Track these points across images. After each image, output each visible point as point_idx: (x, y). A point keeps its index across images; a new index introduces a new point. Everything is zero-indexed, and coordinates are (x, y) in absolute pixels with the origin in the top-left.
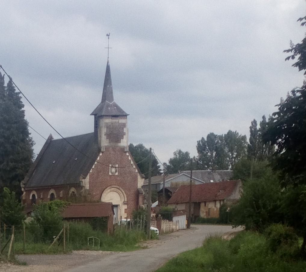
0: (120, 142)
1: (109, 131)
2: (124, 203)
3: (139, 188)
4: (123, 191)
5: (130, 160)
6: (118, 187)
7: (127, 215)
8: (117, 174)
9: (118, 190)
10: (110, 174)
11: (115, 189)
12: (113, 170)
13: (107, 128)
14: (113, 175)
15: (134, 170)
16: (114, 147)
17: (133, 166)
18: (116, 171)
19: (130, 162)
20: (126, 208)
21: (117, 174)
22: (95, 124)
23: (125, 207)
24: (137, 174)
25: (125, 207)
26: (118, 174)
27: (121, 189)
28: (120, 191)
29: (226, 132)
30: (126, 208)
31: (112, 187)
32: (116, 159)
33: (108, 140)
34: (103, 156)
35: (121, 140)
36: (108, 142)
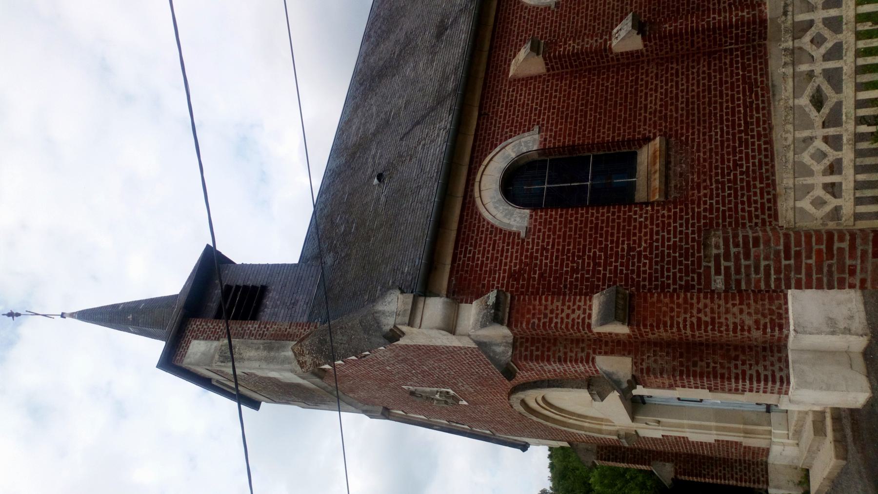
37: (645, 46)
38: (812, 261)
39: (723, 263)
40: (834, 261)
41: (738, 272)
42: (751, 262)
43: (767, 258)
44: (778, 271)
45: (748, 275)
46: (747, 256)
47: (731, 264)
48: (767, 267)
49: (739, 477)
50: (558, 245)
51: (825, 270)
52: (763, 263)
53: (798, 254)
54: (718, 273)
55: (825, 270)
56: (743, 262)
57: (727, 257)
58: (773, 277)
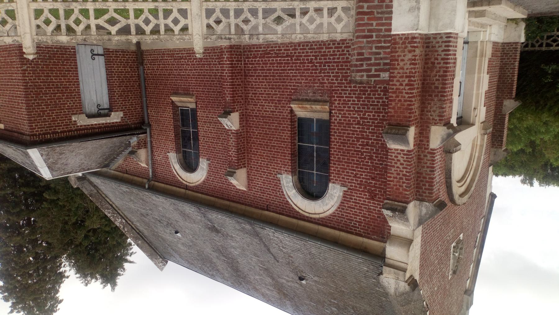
37: (237, 111)
38: (374, 23)
39: (373, 72)
40: (375, 11)
41: (379, 64)
42: (373, 57)
43: (371, 48)
44: (380, 42)
45: (381, 59)
46: (370, 59)
47: (373, 68)
48: (377, 48)
49: (513, 60)
51: (380, 16)
52: (374, 50)
53: (369, 31)
54: (378, 76)
55: (380, 16)
56: (373, 61)
57: (370, 70)
58: (383, 44)
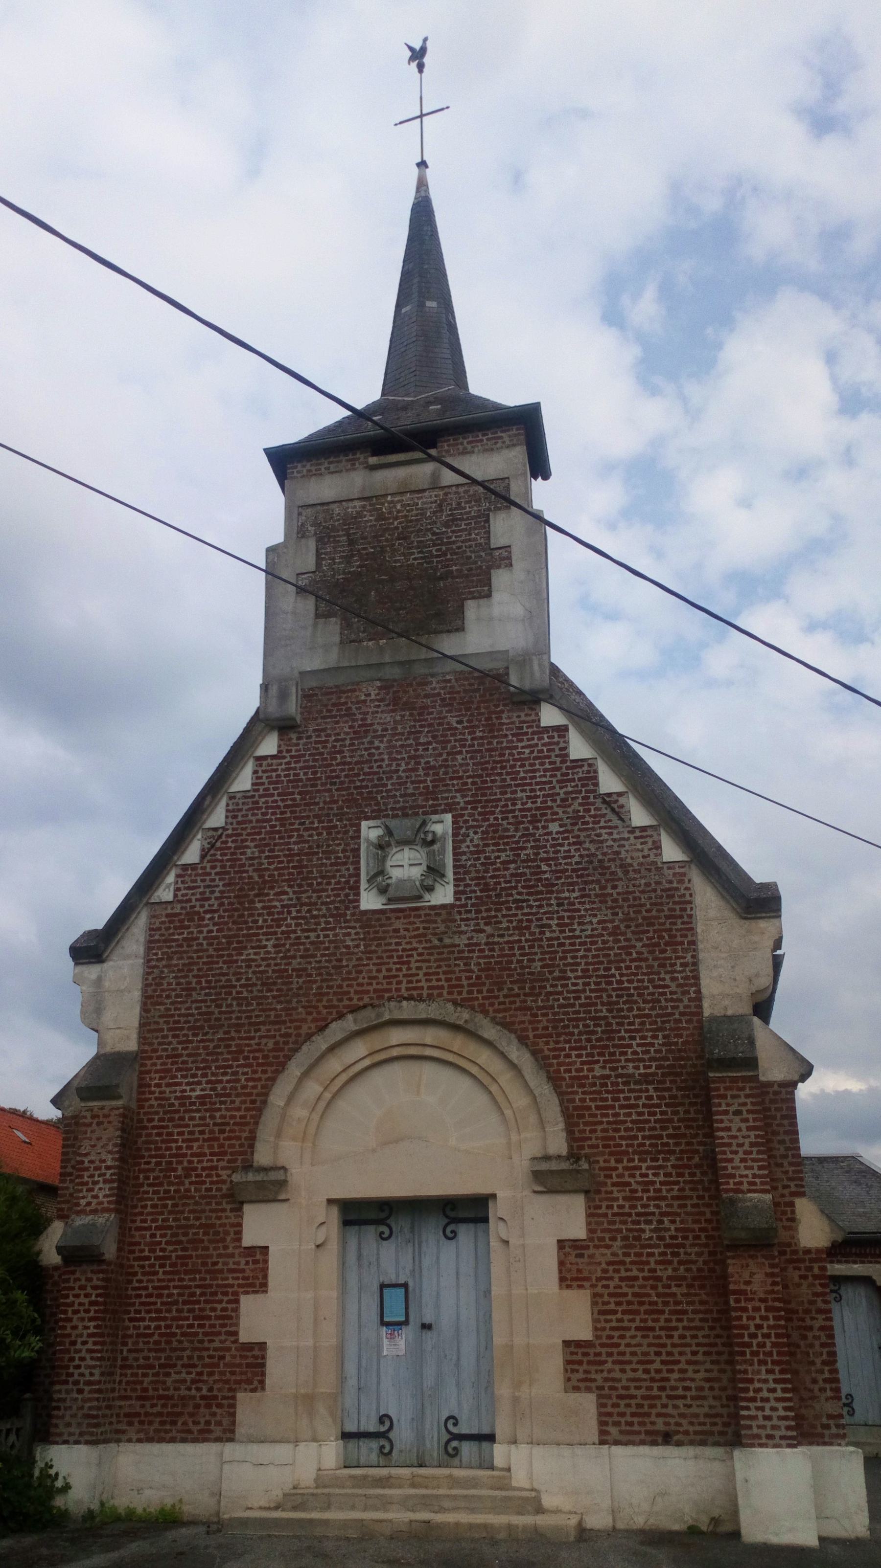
0: (461, 629)
1: (348, 559)
2: (548, 1179)
3: (713, 1019)
4: (515, 1052)
5: (578, 763)
6: (463, 1016)
7: (601, 1312)
8: (443, 895)
9: (458, 1042)
10: (370, 901)
11: (430, 1035)
12: (406, 865)
13: (320, 541)
14: (405, 904)
15: (633, 852)
16: (395, 673)
17: (620, 813)
18: (434, 871)
19: (592, 778)
20: (578, 1230)
21: (443, 895)
22: (267, 608)
23: (570, 1217)
24: (681, 878)
25: (570, 1217)
26: (671, 864)
27: (490, 1032)
28: (485, 1057)
29: (22, 1110)
30: (578, 1230)
31: (387, 1017)
32: (428, 768)
33: (333, 629)
34: (297, 758)
35: (558, 1144)
36: (337, 639)
50: (636, 1098)
